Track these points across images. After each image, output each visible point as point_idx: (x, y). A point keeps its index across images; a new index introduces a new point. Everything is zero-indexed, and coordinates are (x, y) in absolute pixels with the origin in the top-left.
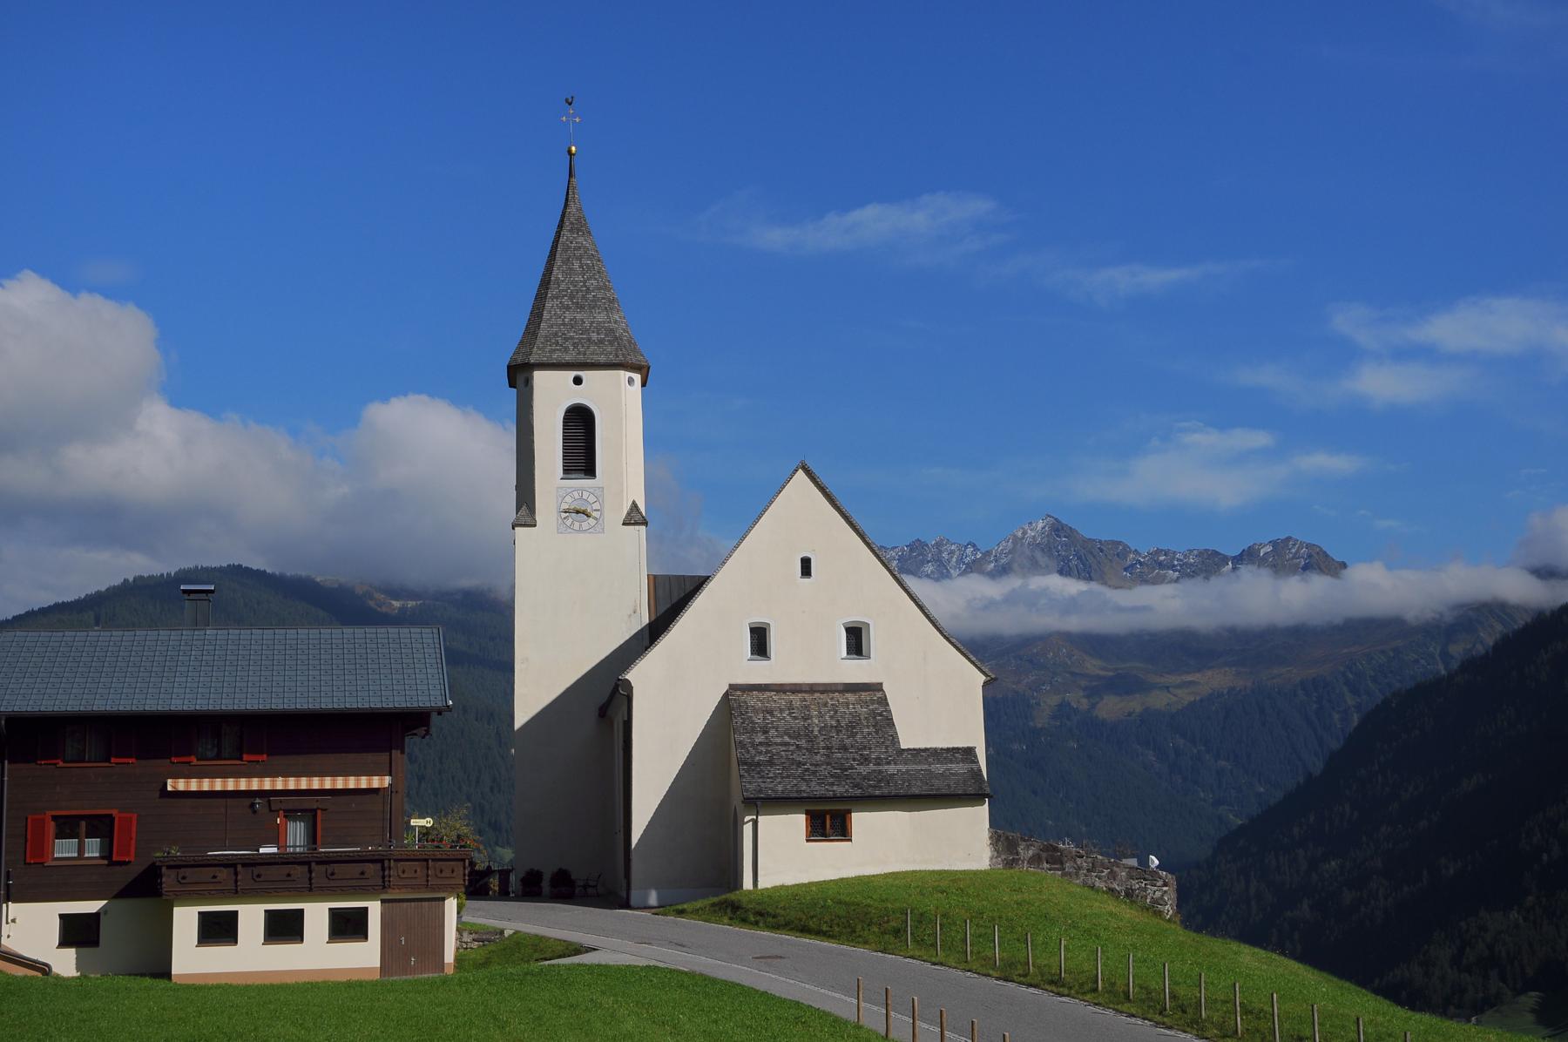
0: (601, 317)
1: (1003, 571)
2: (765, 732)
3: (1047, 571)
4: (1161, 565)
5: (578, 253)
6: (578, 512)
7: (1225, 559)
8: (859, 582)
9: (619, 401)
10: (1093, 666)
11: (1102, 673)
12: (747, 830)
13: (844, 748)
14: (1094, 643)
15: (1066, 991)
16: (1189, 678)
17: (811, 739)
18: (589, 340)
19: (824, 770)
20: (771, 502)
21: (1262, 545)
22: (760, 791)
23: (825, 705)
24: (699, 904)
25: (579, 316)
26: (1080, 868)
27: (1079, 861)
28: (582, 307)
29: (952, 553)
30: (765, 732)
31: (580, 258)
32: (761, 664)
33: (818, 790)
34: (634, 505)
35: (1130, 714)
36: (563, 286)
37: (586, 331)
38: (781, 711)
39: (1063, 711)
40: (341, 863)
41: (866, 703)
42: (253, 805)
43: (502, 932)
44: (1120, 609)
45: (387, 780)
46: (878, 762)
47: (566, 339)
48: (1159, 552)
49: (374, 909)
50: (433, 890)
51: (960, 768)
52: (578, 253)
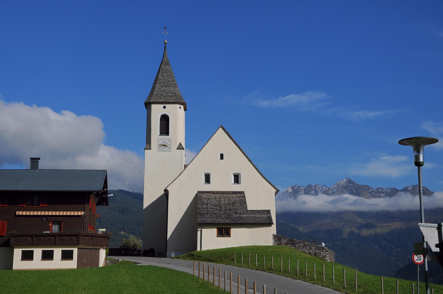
0: (172, 89)
1: (334, 193)
2: (207, 205)
3: (344, 193)
4: (380, 192)
5: (166, 71)
6: (163, 145)
7: (398, 191)
8: (237, 161)
9: (177, 114)
10: (360, 220)
11: (363, 223)
12: (199, 233)
13: (230, 210)
14: (361, 214)
15: (272, 272)
16: (388, 224)
17: (220, 206)
18: (168, 95)
19: (223, 216)
20: (212, 137)
21: (409, 187)
22: (203, 221)
23: (226, 197)
24: (183, 255)
25: (165, 89)
26: (300, 246)
27: (300, 244)
28: (167, 86)
29: (319, 188)
30: (207, 205)
31: (167, 73)
32: (208, 185)
33: (220, 221)
34: (180, 144)
35: (371, 234)
36: (161, 80)
37: (167, 93)
38: (213, 199)
39: (351, 233)
40: (68, 236)
41: (239, 197)
42: (42, 219)
43: (118, 260)
44: (368, 204)
45: (83, 213)
46: (240, 214)
47: (161, 95)
48: (379, 188)
49: (75, 251)
50: (95, 245)
51: (265, 216)
52: (166, 71)
